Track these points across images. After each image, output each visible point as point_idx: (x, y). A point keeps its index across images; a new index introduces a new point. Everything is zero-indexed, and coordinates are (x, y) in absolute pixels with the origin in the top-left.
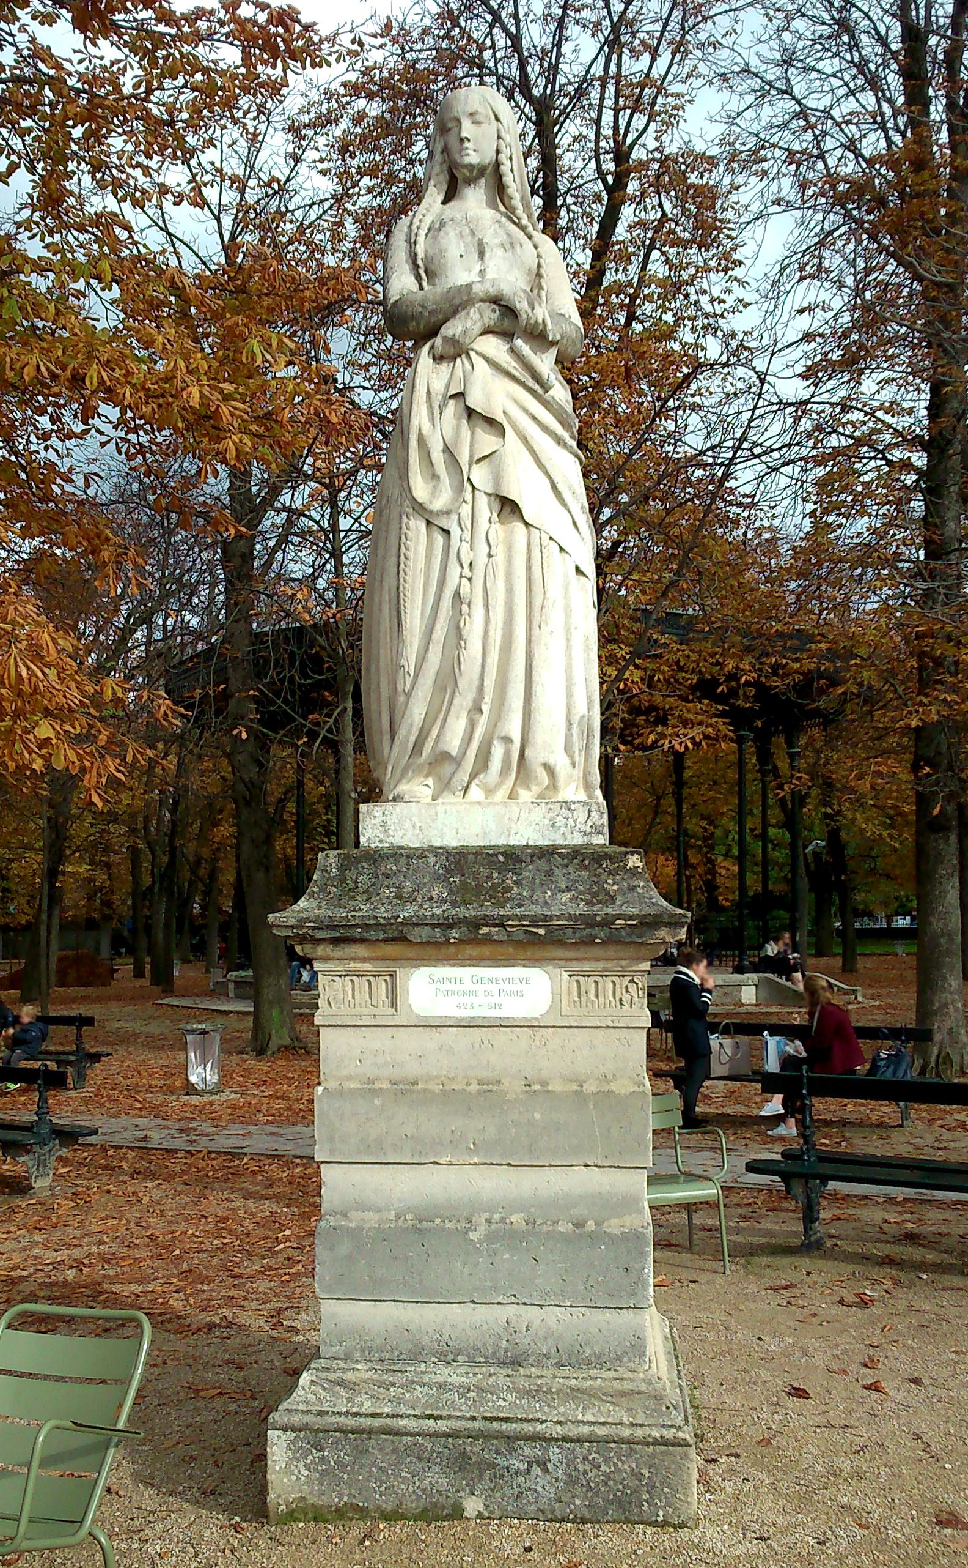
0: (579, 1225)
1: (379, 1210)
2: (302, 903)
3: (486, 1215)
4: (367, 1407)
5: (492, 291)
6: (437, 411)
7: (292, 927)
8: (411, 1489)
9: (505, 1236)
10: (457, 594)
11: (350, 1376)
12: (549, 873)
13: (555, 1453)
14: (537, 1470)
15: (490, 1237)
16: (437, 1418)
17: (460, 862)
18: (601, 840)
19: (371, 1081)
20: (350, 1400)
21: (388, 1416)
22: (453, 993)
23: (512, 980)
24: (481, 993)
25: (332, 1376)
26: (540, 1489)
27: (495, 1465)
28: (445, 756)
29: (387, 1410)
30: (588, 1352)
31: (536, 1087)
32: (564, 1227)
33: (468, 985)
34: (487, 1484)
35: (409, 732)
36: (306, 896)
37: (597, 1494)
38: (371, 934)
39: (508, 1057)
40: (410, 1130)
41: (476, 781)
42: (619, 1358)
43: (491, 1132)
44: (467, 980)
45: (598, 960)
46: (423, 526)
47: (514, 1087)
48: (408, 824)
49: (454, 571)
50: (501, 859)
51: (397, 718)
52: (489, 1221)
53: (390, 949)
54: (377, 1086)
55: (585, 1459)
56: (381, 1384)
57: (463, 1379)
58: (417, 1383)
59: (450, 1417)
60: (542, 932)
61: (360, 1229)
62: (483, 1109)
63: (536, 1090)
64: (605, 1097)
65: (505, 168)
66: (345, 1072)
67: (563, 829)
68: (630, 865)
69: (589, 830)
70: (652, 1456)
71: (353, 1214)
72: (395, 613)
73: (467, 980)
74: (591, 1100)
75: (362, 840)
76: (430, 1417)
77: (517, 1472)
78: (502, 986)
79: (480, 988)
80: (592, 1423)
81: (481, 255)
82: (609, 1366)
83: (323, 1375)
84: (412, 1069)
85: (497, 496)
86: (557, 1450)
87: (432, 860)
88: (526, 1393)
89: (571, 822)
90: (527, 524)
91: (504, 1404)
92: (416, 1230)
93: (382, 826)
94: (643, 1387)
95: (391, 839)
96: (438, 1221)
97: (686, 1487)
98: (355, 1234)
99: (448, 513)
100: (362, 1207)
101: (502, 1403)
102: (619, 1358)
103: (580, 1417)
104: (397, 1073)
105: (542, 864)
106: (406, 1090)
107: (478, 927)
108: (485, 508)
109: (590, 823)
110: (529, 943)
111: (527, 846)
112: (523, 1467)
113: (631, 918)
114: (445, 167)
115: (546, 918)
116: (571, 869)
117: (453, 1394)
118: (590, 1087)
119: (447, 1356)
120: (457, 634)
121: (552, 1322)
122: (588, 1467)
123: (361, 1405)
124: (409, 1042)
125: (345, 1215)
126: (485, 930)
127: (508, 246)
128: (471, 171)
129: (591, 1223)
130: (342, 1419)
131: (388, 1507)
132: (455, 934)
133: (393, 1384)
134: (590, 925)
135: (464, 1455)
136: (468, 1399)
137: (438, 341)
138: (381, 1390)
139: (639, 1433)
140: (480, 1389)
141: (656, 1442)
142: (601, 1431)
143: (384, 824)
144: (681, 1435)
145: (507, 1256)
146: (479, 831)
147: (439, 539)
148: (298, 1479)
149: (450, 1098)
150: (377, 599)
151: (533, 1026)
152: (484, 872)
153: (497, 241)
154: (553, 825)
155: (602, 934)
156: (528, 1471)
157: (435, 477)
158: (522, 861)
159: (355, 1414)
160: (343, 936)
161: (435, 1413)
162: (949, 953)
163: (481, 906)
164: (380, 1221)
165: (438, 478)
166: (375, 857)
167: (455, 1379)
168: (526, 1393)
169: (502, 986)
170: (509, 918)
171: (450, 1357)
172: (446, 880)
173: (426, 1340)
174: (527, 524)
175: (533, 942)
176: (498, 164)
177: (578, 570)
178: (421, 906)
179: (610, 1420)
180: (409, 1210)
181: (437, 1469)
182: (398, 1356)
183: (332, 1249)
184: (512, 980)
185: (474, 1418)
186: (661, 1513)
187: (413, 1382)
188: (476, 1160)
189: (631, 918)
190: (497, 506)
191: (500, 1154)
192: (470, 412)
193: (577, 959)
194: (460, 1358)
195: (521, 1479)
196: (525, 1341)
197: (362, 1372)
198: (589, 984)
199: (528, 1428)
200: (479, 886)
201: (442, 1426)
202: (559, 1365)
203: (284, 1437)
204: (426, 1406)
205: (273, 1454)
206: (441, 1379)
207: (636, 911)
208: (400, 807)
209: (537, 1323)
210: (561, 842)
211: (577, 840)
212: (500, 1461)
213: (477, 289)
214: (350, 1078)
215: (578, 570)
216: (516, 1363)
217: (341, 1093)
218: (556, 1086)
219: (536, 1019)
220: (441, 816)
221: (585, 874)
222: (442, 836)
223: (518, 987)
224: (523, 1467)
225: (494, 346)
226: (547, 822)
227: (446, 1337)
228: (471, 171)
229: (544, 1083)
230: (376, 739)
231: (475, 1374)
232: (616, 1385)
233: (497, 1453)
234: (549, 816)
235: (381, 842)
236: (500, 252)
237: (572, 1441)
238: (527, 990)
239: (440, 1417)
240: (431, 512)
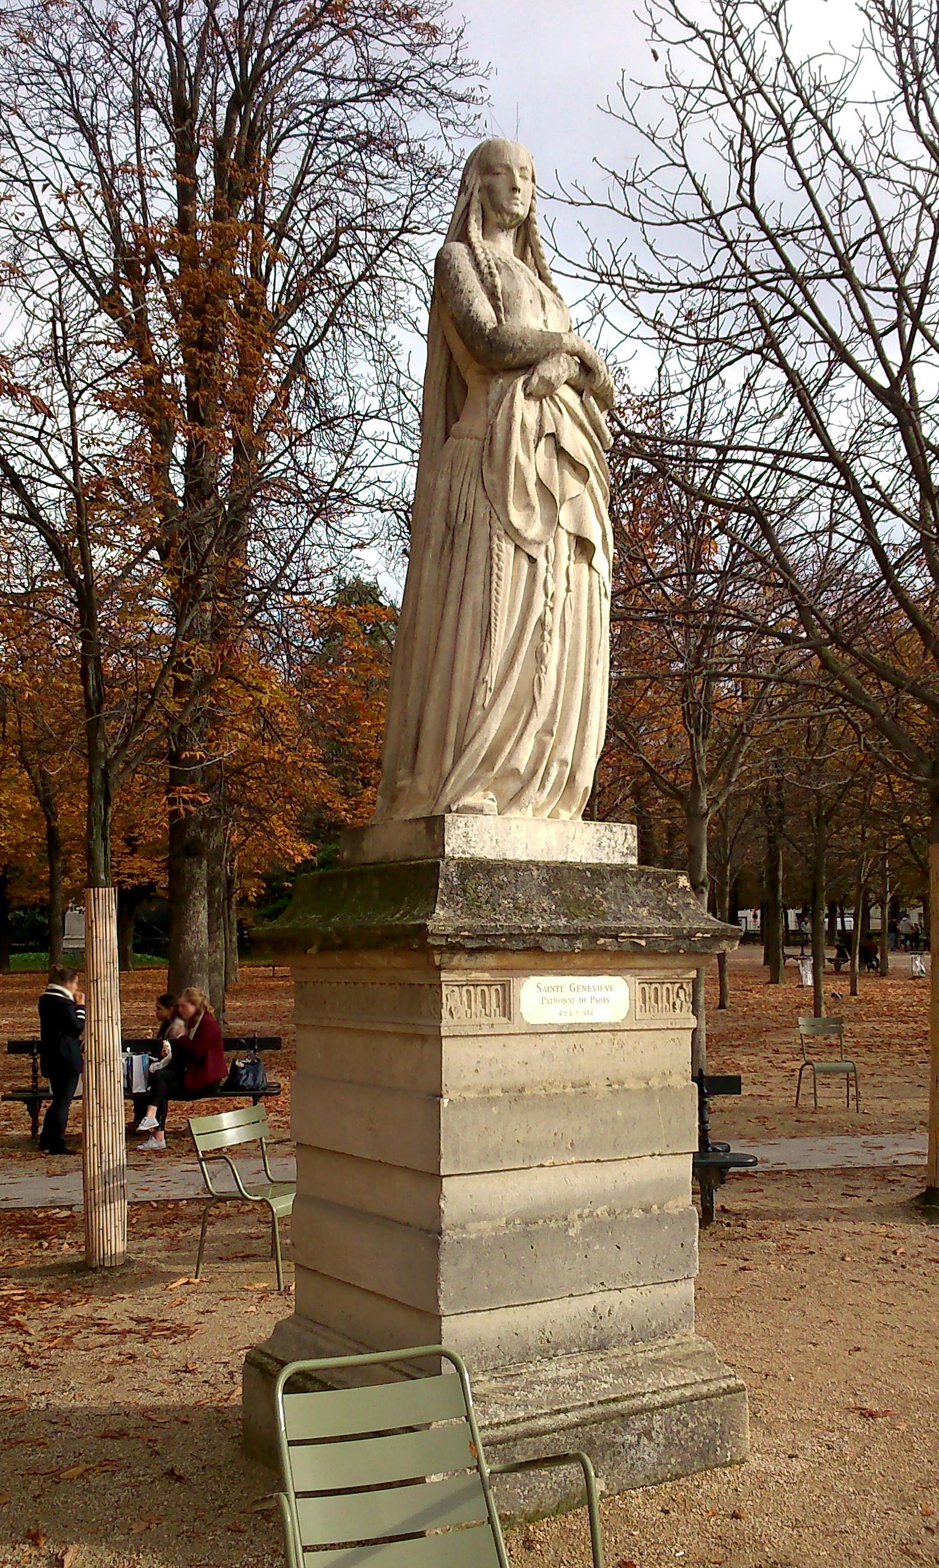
1: (491, 1218)
3: (578, 1211)
4: (503, 1417)
5: (578, 347)
6: (532, 445)
7: (448, 936)
9: (597, 1228)
10: (541, 623)
13: (657, 1421)
15: (584, 1232)
16: (566, 1411)
18: (633, 861)
19: (486, 1090)
21: (524, 1420)
23: (600, 988)
28: (515, 772)
29: (522, 1414)
30: (654, 1324)
33: (567, 994)
35: (482, 746)
37: (685, 1450)
38: (514, 944)
39: (595, 1060)
40: (521, 1136)
42: (675, 1327)
44: (566, 989)
46: (512, 549)
47: (599, 1086)
48: (486, 837)
49: (540, 599)
53: (516, 959)
54: (491, 1094)
55: (678, 1420)
59: (574, 1408)
60: (643, 943)
61: (480, 1238)
62: (569, 1107)
63: (616, 1087)
70: (723, 1405)
71: (471, 1226)
76: (559, 1412)
77: (631, 1446)
79: (577, 995)
80: (677, 1388)
84: (521, 1077)
87: (535, 873)
88: (620, 1372)
89: (613, 843)
91: (606, 1386)
95: (472, 851)
96: (541, 1222)
98: (475, 1245)
99: (539, 543)
100: (478, 1217)
101: (604, 1385)
104: (507, 1081)
105: (618, 880)
108: (565, 544)
110: (635, 953)
112: (634, 1439)
116: (640, 887)
117: (560, 1391)
119: (549, 1350)
120: (539, 656)
124: (519, 1049)
125: (463, 1228)
126: (601, 941)
129: (655, 1207)
131: (530, 1510)
132: (579, 944)
133: (516, 1388)
134: (677, 938)
138: (508, 1397)
139: (713, 1387)
140: (586, 1377)
142: (688, 1392)
143: (466, 835)
146: (543, 846)
147: (525, 564)
155: (684, 945)
157: (529, 506)
159: (498, 1425)
160: (484, 945)
161: (563, 1406)
162: (200, 969)
163: (565, 922)
164: (494, 1229)
165: (533, 508)
168: (620, 1372)
169: (593, 993)
171: (552, 1352)
172: (549, 892)
173: (532, 1341)
174: (590, 565)
182: (511, 1361)
184: (600, 988)
185: (592, 1404)
187: (532, 1382)
188: (573, 1159)
193: (648, 968)
198: (650, 991)
199: (637, 1403)
200: (577, 899)
201: (573, 1417)
202: (634, 1341)
204: (551, 1403)
210: (605, 861)
211: (617, 860)
214: (468, 1088)
216: (602, 1347)
218: (630, 1084)
220: (514, 829)
221: (650, 890)
222: (514, 849)
224: (634, 1439)
227: (547, 1334)
229: (621, 1083)
235: (463, 852)
237: (668, 1406)
238: (604, 997)
239: (566, 1411)
240: (525, 539)
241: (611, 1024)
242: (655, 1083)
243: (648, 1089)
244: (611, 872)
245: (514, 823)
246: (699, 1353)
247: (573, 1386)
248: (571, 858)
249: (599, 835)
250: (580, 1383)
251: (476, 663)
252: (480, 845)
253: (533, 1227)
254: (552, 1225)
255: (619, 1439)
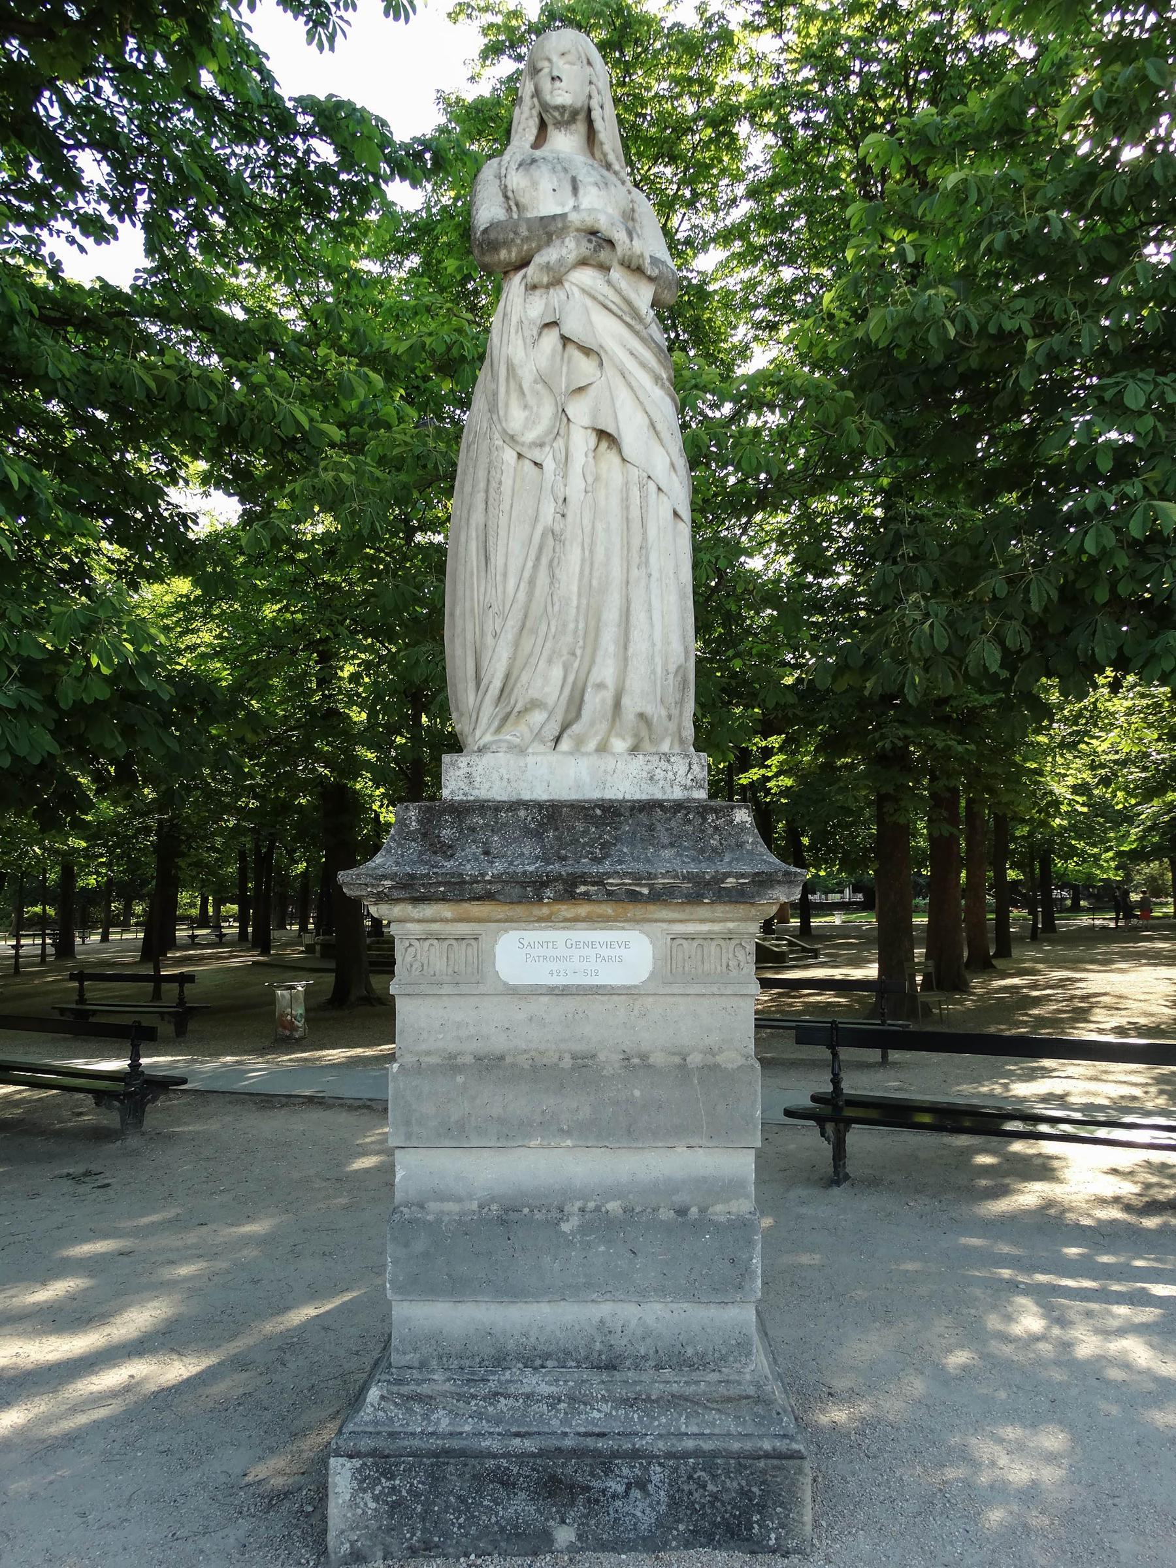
0: (682, 1212)
1: (459, 1200)
2: (378, 859)
3: (579, 1204)
4: (444, 1425)
5: (589, 221)
8: (493, 1519)
11: (425, 1389)
12: (651, 828)
14: (636, 1493)
15: (583, 1229)
17: (552, 816)
18: (701, 794)
20: (426, 1417)
22: (545, 958)
24: (576, 959)
25: (405, 1390)
26: (639, 1514)
27: (588, 1488)
29: (467, 1428)
31: (636, 1061)
32: (666, 1214)
34: (580, 1508)
36: (382, 852)
39: (605, 1032)
40: (496, 1111)
41: (569, 732)
43: (586, 1112)
44: (561, 944)
45: (703, 921)
47: (610, 1060)
48: (495, 776)
50: (598, 812)
51: (485, 664)
52: (582, 1210)
55: (690, 1477)
56: (460, 1396)
57: (553, 1388)
58: (502, 1394)
60: (645, 891)
61: (439, 1221)
63: (637, 1064)
64: (711, 1070)
65: (596, 114)
66: (424, 1047)
67: (661, 782)
68: (738, 820)
69: (689, 783)
70: (764, 1472)
71: (433, 1206)
72: (482, 552)
73: (561, 944)
74: (693, 1074)
75: (446, 793)
77: (615, 1496)
78: (599, 950)
81: (575, 190)
82: (712, 1366)
83: (395, 1389)
84: (499, 1043)
85: (594, 429)
86: (658, 1469)
90: (624, 460)
91: (597, 1415)
92: (503, 1222)
93: (460, 779)
94: (751, 1391)
96: (526, 1211)
97: (799, 1503)
100: (441, 1197)
101: (595, 1414)
102: (723, 1358)
103: (683, 1429)
106: (491, 1065)
107: (574, 885)
108: (581, 441)
109: (690, 776)
111: (624, 801)
113: (743, 876)
114: (535, 113)
115: (650, 876)
116: (673, 824)
118: (695, 1059)
119: (533, 1360)
121: (650, 1320)
122: (693, 1487)
123: (438, 1423)
125: (421, 1206)
127: (602, 185)
128: (562, 114)
129: (694, 1210)
130: (416, 1443)
133: (474, 1397)
135: (553, 1478)
136: (558, 1411)
137: (530, 270)
140: (572, 1399)
141: (767, 1456)
142: (707, 1446)
143: (469, 776)
144: (795, 1446)
145: (602, 1248)
148: (364, 1513)
149: (539, 1073)
150: (463, 539)
151: (628, 992)
152: (579, 826)
153: (592, 180)
154: (651, 779)
156: (627, 1492)
158: (620, 815)
161: (523, 1430)
166: (461, 810)
167: (545, 1389)
169: (599, 950)
170: (609, 875)
171: (538, 1362)
174: (624, 460)
175: (635, 897)
176: (589, 111)
177: (676, 514)
178: (511, 863)
179: (717, 1431)
180: (493, 1199)
181: (523, 1495)
183: (406, 1245)
186: (773, 1536)
189: (743, 876)
190: (593, 438)
191: (594, 1132)
192: (565, 340)
193: (681, 921)
194: (549, 1363)
195: (618, 1503)
196: (619, 1342)
197: (439, 1382)
201: (529, 1445)
202: (658, 1367)
203: (349, 1465)
205: (336, 1485)
206: (528, 1390)
207: (747, 869)
208: (487, 759)
209: (634, 1322)
211: (677, 794)
212: (596, 1484)
213: (573, 217)
214: (428, 1053)
215: (676, 514)
216: (611, 1367)
217: (418, 1069)
219: (635, 987)
221: (689, 828)
223: (616, 952)
224: (621, 1489)
225: (586, 277)
226: (645, 774)
227: (533, 1340)
228: (562, 114)
229: (644, 1057)
230: (460, 687)
231: (566, 1382)
232: (722, 1389)
233: (592, 1474)
234: (646, 768)
236: (594, 190)
238: (613, 953)
240: (523, 445)
241: (624, 987)
242: (695, 1059)
243: (683, 1067)
244: (632, 808)
245: (530, 760)
246: (748, 1397)
247: (552, 1406)
248: (610, 795)
249: (650, 767)
250: (562, 1406)
251: (482, 589)
252: (487, 786)
253: (514, 1216)
254: (538, 1216)
255: (596, 1484)
